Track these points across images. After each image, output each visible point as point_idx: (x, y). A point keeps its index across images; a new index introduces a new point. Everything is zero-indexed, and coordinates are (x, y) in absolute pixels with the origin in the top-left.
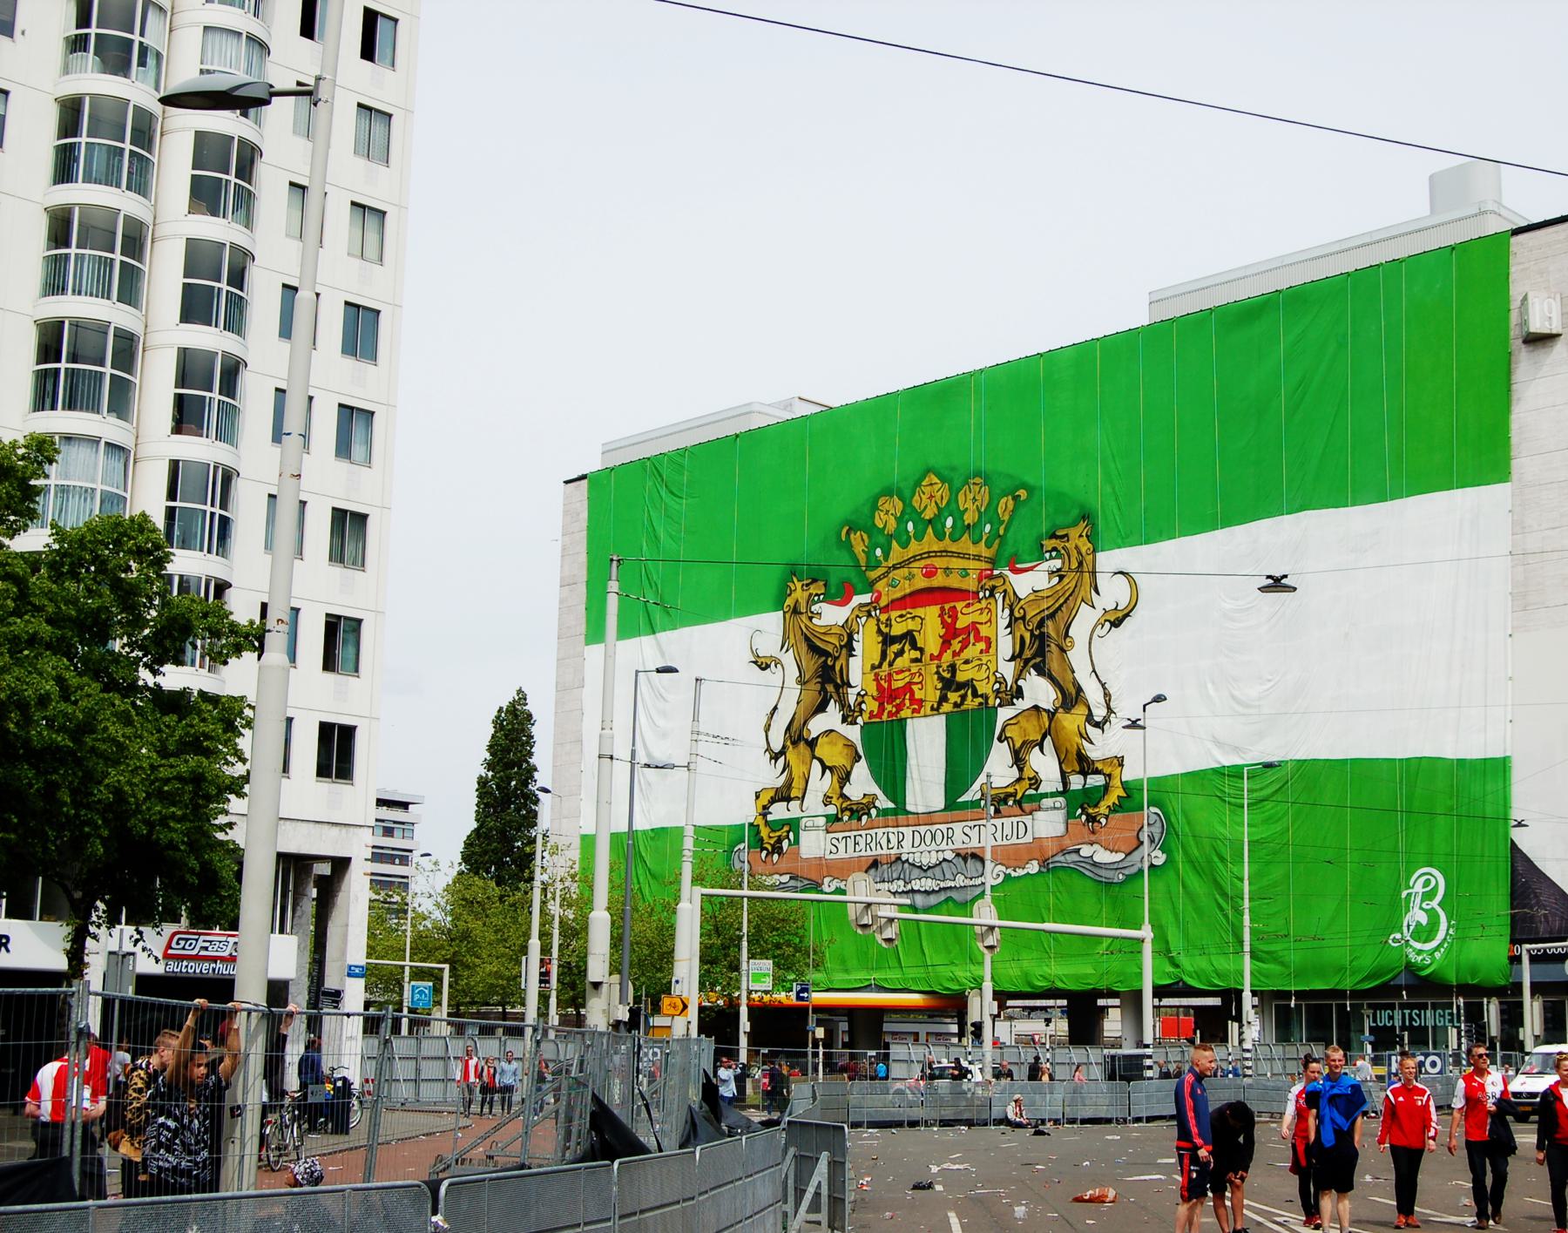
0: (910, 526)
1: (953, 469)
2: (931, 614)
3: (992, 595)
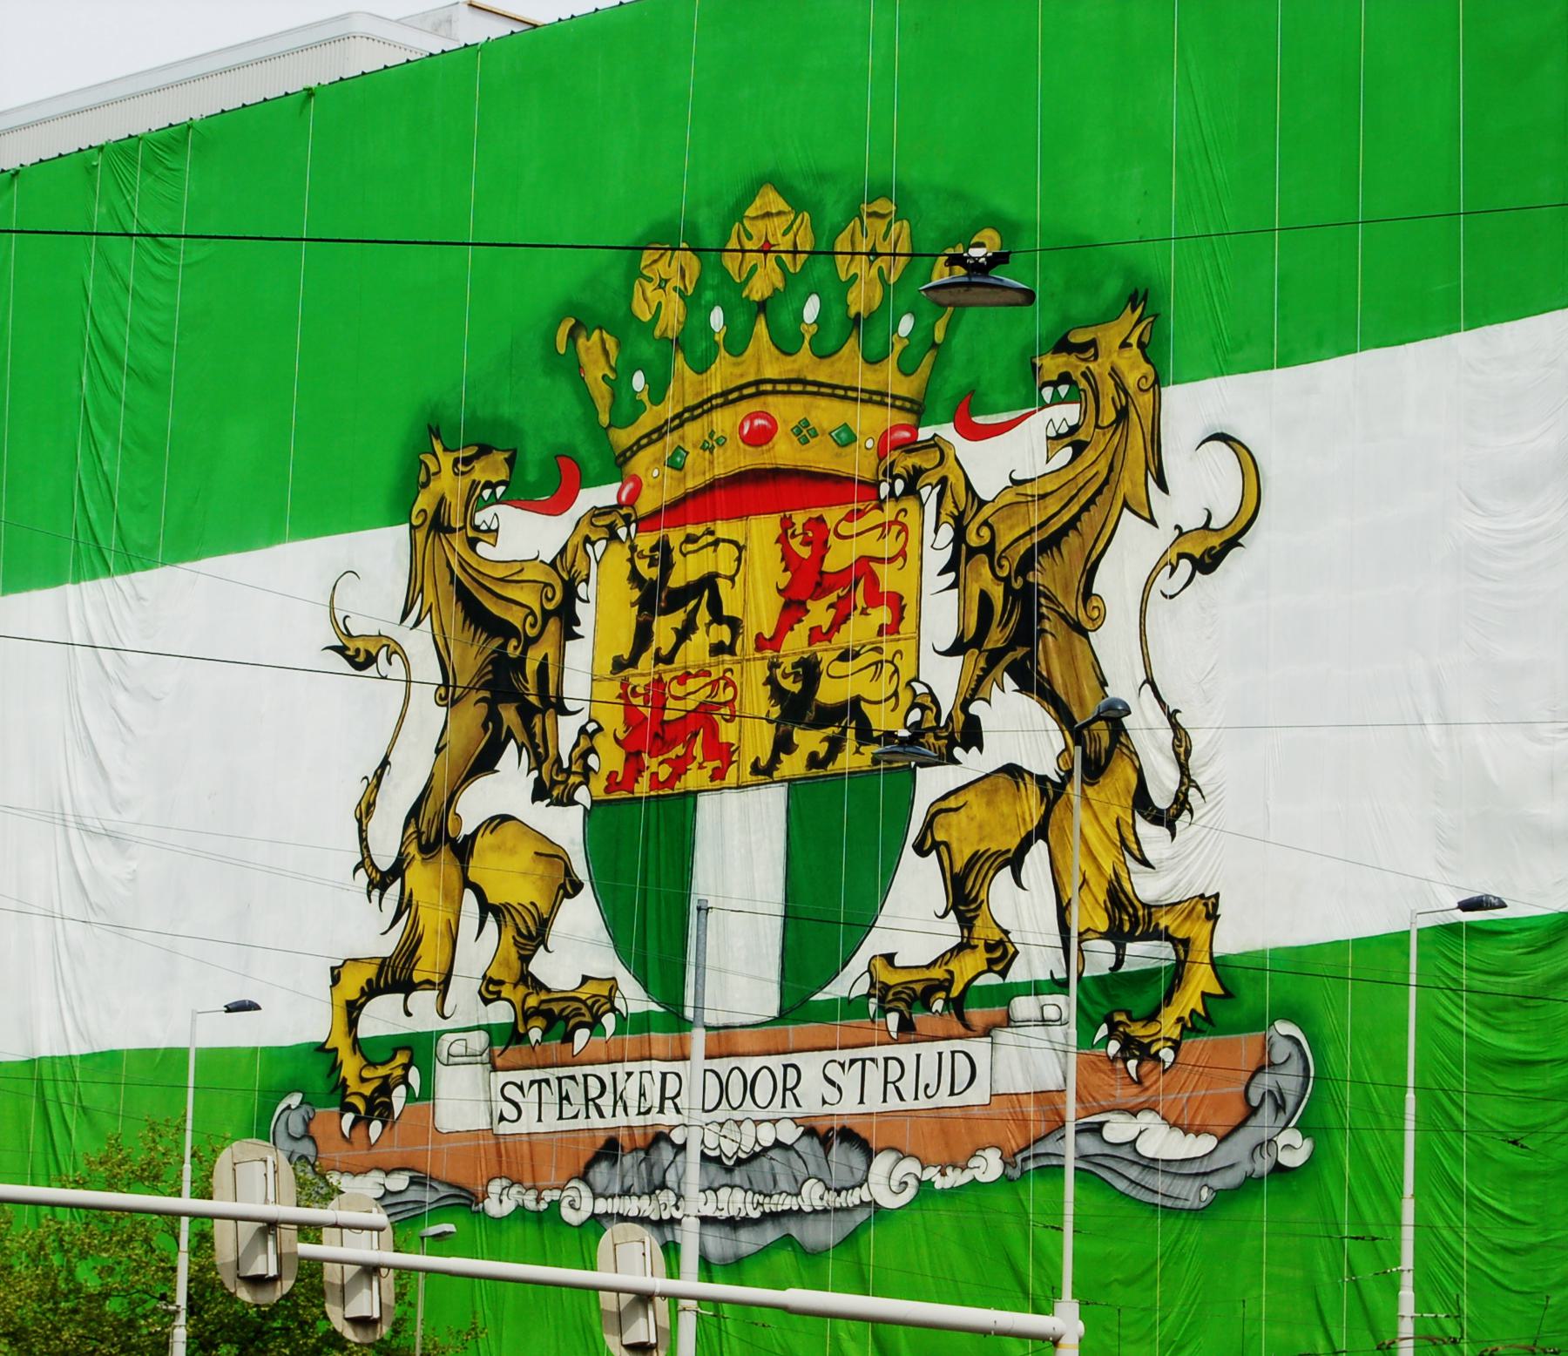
0: (717, 318)
1: (822, 177)
2: (762, 531)
3: (911, 490)
